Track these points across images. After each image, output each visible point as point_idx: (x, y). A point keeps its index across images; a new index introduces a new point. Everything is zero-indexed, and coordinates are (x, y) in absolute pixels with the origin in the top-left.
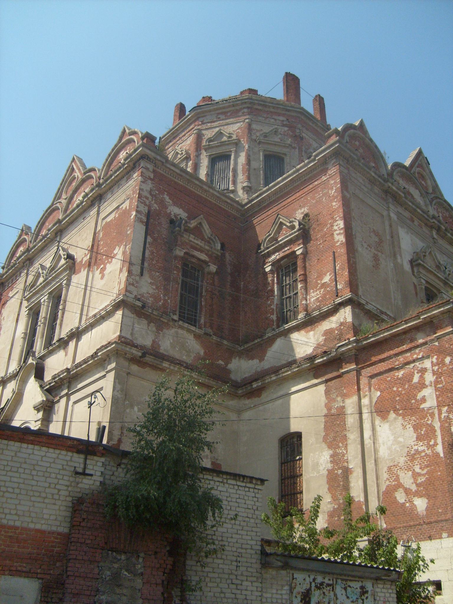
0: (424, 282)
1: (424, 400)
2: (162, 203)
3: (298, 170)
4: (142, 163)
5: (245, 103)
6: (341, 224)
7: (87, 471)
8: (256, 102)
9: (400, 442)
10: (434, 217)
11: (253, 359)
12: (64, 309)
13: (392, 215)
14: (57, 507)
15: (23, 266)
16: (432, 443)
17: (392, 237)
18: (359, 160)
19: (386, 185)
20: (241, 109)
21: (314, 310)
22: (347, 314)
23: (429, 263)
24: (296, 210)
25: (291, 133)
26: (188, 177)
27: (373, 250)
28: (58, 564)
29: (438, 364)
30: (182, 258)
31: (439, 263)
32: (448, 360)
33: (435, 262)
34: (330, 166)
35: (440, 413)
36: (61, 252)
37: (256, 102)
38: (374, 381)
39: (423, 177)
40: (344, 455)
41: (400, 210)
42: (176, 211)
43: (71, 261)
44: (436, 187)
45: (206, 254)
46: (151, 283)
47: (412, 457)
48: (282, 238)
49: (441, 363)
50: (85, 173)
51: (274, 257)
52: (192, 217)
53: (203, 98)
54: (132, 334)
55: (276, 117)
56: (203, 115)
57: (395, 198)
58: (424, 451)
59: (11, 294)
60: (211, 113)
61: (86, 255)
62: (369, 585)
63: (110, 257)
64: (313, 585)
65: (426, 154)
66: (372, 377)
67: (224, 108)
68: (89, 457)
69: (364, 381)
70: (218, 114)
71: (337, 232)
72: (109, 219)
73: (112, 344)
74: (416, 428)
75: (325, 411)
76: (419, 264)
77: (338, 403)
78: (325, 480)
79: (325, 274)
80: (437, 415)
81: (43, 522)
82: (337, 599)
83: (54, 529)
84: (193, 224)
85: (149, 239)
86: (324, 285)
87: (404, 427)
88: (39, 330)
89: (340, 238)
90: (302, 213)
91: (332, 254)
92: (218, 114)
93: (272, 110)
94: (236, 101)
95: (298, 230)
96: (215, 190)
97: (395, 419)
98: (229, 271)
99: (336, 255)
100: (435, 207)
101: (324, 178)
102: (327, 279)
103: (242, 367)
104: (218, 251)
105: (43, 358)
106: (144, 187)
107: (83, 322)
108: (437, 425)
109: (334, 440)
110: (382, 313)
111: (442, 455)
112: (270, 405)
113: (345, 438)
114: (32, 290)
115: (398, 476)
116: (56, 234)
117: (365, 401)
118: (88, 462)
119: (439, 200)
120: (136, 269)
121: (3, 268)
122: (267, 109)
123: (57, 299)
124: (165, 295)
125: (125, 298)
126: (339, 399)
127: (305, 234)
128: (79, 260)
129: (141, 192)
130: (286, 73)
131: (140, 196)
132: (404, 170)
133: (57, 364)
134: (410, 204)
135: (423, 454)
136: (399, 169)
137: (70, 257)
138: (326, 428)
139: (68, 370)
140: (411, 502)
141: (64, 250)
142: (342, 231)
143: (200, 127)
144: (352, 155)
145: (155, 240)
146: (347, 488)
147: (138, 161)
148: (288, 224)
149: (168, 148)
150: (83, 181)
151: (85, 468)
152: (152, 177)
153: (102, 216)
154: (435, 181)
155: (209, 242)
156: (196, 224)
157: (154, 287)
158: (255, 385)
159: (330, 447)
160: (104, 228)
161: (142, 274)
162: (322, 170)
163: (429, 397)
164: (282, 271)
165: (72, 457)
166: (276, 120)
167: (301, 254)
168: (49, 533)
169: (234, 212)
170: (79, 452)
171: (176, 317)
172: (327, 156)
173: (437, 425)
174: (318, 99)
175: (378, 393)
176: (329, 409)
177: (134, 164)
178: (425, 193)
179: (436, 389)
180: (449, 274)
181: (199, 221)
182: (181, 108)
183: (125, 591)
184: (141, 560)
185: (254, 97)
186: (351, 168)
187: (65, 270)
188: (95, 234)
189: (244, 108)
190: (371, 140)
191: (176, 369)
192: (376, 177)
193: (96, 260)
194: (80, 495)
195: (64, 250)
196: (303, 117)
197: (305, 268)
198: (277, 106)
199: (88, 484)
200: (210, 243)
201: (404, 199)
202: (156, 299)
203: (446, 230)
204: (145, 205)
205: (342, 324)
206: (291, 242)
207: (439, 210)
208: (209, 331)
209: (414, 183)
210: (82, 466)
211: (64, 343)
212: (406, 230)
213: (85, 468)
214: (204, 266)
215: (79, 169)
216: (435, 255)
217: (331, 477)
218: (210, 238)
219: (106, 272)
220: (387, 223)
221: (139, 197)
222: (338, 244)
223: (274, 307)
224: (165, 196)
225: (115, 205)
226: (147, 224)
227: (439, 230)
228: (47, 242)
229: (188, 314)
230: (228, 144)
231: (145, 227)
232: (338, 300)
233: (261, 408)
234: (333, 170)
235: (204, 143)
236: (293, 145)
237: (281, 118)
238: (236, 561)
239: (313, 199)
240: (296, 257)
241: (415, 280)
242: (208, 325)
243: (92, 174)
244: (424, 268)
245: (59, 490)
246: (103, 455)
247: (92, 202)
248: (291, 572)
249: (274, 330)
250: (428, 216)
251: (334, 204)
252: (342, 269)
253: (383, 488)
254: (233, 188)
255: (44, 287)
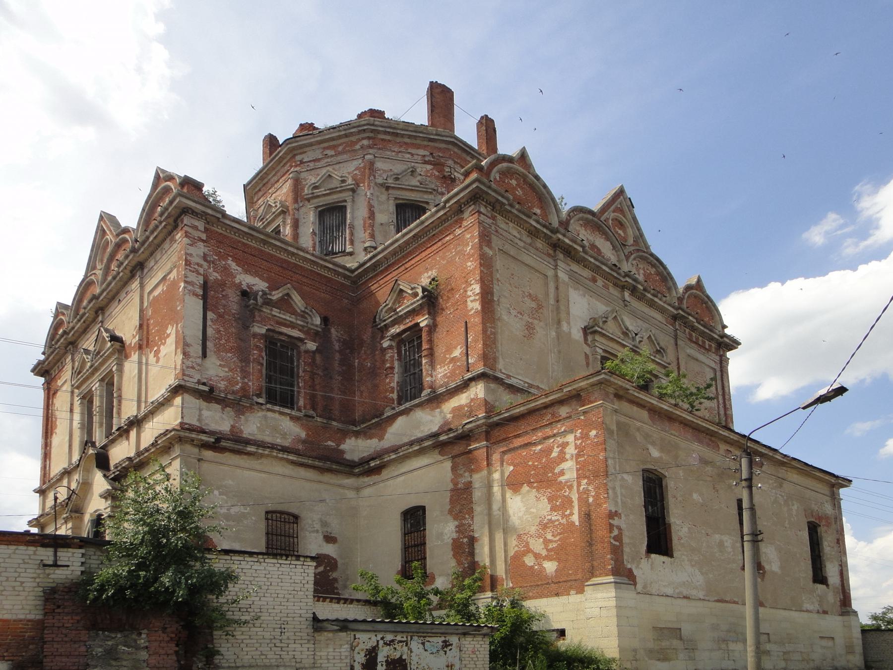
0: (600, 351)
1: (562, 473)
2: (226, 270)
3: (423, 222)
4: (187, 220)
5: (364, 130)
6: (477, 288)
7: (59, 563)
8: (381, 129)
9: (532, 513)
10: (627, 275)
11: (371, 438)
12: (120, 396)
13: (561, 274)
14: (21, 598)
15: (66, 353)
16: (568, 512)
17: (558, 301)
18: (511, 205)
19: (554, 236)
20: (359, 140)
21: (441, 386)
22: (478, 390)
23: (611, 328)
24: (421, 273)
25: (437, 173)
26: (262, 237)
27: (526, 318)
28: (31, 647)
29: (582, 438)
30: (265, 337)
31: (627, 329)
32: (593, 433)
33: (621, 328)
34: (466, 215)
35: (579, 485)
36: (105, 334)
37: (381, 129)
38: (506, 457)
39: (621, 225)
40: (470, 526)
41: (575, 267)
42: (247, 280)
43: (118, 345)
44: (640, 237)
45: (300, 330)
46: (220, 365)
47: (544, 526)
48: (402, 309)
49: (585, 436)
50: (118, 235)
51: (395, 330)
52: (273, 287)
53: (301, 125)
54: (199, 420)
55: (413, 151)
56: (301, 151)
57: (569, 253)
58: (558, 520)
59: (60, 383)
60: (314, 147)
61: (134, 337)
62: (454, 640)
63: (163, 338)
64: (381, 642)
65: (629, 193)
66: (504, 453)
67: (333, 139)
68: (59, 550)
69: (496, 457)
70: (325, 148)
71: (472, 298)
72: (156, 293)
73: (171, 431)
74: (550, 500)
75: (451, 486)
76: (595, 332)
77: (466, 477)
78: (450, 547)
79: (455, 348)
80: (575, 487)
81: (5, 612)
82: (411, 652)
83: (22, 617)
84: (276, 295)
85: (210, 315)
86: (453, 360)
87: (538, 499)
88: (96, 419)
89: (474, 305)
90: (429, 277)
91: (464, 324)
92: (325, 148)
93: (407, 140)
94: (350, 129)
95: (422, 298)
96: (307, 252)
97: (528, 491)
98: (337, 347)
99: (469, 325)
100: (634, 262)
101: (458, 232)
102: (457, 352)
103: (356, 448)
104: (317, 326)
105: (104, 447)
106: (192, 250)
107: (143, 409)
108: (575, 497)
109: (460, 512)
110: (531, 386)
111: (577, 523)
112: (391, 482)
113: (471, 510)
114: (81, 377)
115: (527, 543)
116: (96, 312)
117: (496, 476)
118: (59, 554)
119: (641, 254)
120: (196, 350)
121: (44, 353)
122: (399, 140)
123: (109, 384)
124: (243, 378)
125: (183, 383)
126: (467, 474)
127: (431, 300)
128: (128, 343)
129: (189, 258)
130: (431, 83)
131: (188, 263)
132: (590, 217)
133: (120, 452)
134: (592, 260)
135: (557, 523)
136: (581, 215)
137: (114, 338)
138: (452, 501)
139: (129, 459)
140: (540, 565)
141: (107, 330)
142: (477, 297)
143: (298, 169)
144: (500, 198)
145: (220, 316)
146: (472, 554)
147: (179, 216)
148: (410, 292)
149: (258, 200)
150: (118, 246)
151: (56, 561)
152: (204, 237)
153: (148, 289)
154: (639, 229)
155: (303, 316)
156: (280, 295)
157: (227, 369)
158: (372, 464)
159: (455, 519)
160: (150, 304)
161: (204, 355)
162: (456, 221)
163: (569, 469)
164: (405, 345)
165: (35, 552)
166: (412, 155)
167: (426, 326)
168: (14, 621)
169: (340, 279)
170: (44, 545)
171: (261, 400)
172: (462, 201)
173: (575, 497)
174: (484, 121)
175: (512, 468)
176: (456, 484)
177: (175, 221)
178: (619, 245)
179: (577, 463)
180: (640, 341)
181: (286, 292)
182: (271, 142)
183: (124, 663)
184: (144, 636)
185: (378, 121)
186: (499, 217)
187: (112, 354)
188: (142, 311)
189: (363, 139)
190: (537, 177)
191: (266, 452)
192: (538, 226)
193: (148, 342)
194: (54, 585)
195: (107, 330)
196: (456, 150)
197: (430, 341)
198: (414, 134)
199: (60, 575)
200: (306, 318)
201: (582, 254)
202: (231, 381)
203: (645, 290)
204: (199, 274)
205: (472, 400)
206: (414, 312)
207: (641, 266)
208: (311, 412)
209: (604, 233)
210: (52, 558)
211: (124, 432)
212: (581, 292)
213: (56, 561)
214: (300, 344)
215: (110, 231)
216: (622, 320)
217: (457, 546)
218: (304, 312)
219: (161, 355)
220: (552, 286)
221: (186, 265)
222: (472, 312)
223: (394, 384)
224: (230, 262)
225: (160, 275)
226: (205, 298)
227: (634, 291)
228: (87, 322)
229: (280, 396)
230: (340, 192)
231: (201, 302)
232: (468, 375)
233: (382, 485)
234: (470, 219)
235: (307, 191)
236: (440, 190)
237: (422, 152)
238: (281, 628)
239: (443, 259)
240: (421, 329)
241: (587, 350)
242: (308, 407)
243: (127, 236)
244: (603, 335)
245: (22, 583)
246: (80, 547)
247: (131, 272)
248: (353, 633)
249: (394, 408)
250: (618, 274)
251: (469, 264)
252: (475, 341)
253: (511, 553)
254: (351, 250)
255: (93, 374)
